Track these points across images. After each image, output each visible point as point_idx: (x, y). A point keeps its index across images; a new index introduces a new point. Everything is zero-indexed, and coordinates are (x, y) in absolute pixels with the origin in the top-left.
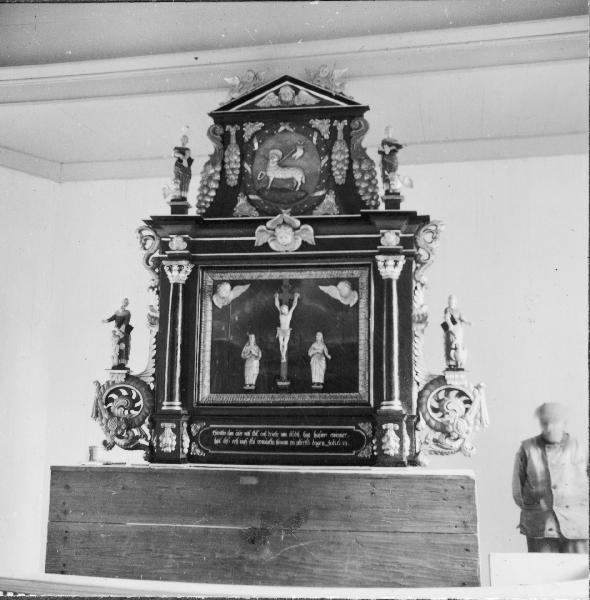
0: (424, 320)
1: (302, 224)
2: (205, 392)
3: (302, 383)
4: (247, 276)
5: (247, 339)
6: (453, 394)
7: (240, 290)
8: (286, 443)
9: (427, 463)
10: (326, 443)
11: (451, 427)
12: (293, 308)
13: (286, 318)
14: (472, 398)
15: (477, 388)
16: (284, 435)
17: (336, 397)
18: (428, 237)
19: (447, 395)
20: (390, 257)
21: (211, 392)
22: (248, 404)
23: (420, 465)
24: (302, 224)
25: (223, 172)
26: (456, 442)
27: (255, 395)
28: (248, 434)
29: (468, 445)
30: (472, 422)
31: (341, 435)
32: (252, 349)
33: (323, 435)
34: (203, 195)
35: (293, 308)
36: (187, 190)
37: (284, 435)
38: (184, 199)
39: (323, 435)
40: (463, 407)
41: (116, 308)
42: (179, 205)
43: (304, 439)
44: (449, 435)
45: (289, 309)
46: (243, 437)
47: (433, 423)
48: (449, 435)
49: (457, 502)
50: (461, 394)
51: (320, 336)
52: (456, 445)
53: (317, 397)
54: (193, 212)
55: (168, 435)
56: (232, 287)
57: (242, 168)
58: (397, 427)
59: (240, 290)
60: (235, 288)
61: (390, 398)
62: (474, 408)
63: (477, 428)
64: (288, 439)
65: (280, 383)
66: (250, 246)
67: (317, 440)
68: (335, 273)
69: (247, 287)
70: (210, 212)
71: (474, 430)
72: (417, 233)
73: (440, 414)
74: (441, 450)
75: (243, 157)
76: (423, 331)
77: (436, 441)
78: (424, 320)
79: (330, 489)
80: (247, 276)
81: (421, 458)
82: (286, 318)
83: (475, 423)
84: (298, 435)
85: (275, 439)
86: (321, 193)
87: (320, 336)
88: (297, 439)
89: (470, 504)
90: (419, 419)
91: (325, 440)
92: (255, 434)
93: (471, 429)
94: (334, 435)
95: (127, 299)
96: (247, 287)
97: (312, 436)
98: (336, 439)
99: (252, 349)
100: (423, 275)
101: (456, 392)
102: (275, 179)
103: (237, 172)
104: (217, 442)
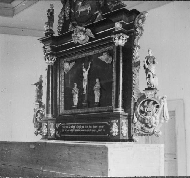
0: (138, 63)
1: (86, 29)
2: (62, 110)
3: (91, 103)
4: (74, 58)
5: (73, 86)
6: (151, 103)
7: (73, 64)
8: (84, 130)
9: (137, 141)
10: (97, 130)
11: (146, 120)
12: (88, 69)
13: (85, 74)
14: (159, 104)
15: (162, 98)
16: (83, 127)
17: (103, 108)
18: (140, 21)
19: (148, 104)
20: (116, 35)
21: (65, 110)
22: (73, 114)
23: (135, 142)
24: (86, 29)
25: (64, 15)
26: (151, 129)
27: (77, 110)
28: (72, 127)
29: (156, 130)
30: (158, 118)
31: (103, 127)
32: (75, 90)
33: (96, 127)
34: (59, 26)
35: (88, 69)
36: (52, 26)
37: (83, 127)
38: (51, 30)
39: (96, 127)
40: (155, 109)
41: (37, 80)
42: (50, 32)
43: (90, 129)
44: (147, 126)
45: (87, 70)
46: (71, 129)
47: (140, 119)
48: (147, 126)
49: (100, 161)
50: (155, 103)
51: (97, 80)
52: (151, 130)
53: (97, 109)
54: (56, 35)
55: (44, 128)
56: (69, 64)
57: (70, 12)
58: (117, 121)
59: (73, 64)
60: (71, 64)
61: (117, 106)
62: (160, 109)
63: (163, 121)
64: (84, 129)
65: (83, 104)
66: (73, 44)
67: (94, 129)
68: (100, 51)
69: (74, 62)
70: (61, 32)
71: (160, 122)
72: (134, 21)
73: (144, 114)
74: (143, 133)
75: (70, 7)
76: (138, 71)
77: (142, 128)
78: (138, 63)
79: (65, 154)
80: (74, 58)
81: (134, 137)
82: (85, 74)
83: (160, 118)
84: (87, 127)
85: (80, 129)
86: (97, 12)
87: (97, 80)
88: (87, 129)
89: (105, 162)
90: (134, 117)
91: (97, 129)
92: (74, 127)
93: (158, 121)
94: (100, 127)
95: (42, 75)
96: (74, 62)
97: (92, 127)
98: (101, 128)
99: (75, 90)
100: (138, 42)
101: (153, 102)
102: (81, 12)
103: (68, 13)
104: (63, 130)
